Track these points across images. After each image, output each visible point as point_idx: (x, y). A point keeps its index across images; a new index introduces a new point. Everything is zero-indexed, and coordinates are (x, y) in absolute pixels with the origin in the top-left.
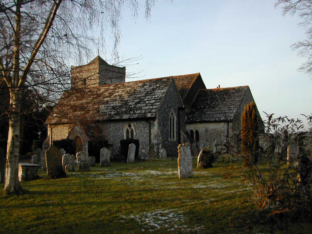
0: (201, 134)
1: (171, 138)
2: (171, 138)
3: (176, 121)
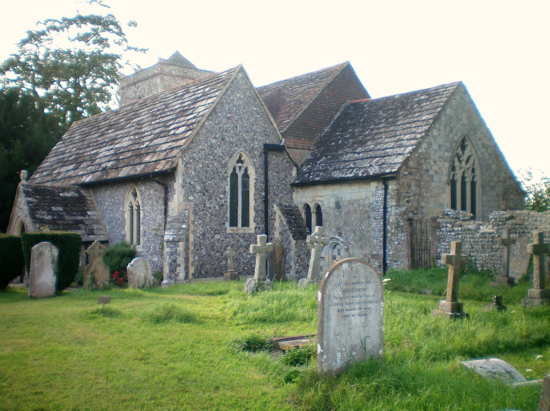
0: (327, 213)
1: (234, 223)
2: (234, 223)
3: (256, 179)
